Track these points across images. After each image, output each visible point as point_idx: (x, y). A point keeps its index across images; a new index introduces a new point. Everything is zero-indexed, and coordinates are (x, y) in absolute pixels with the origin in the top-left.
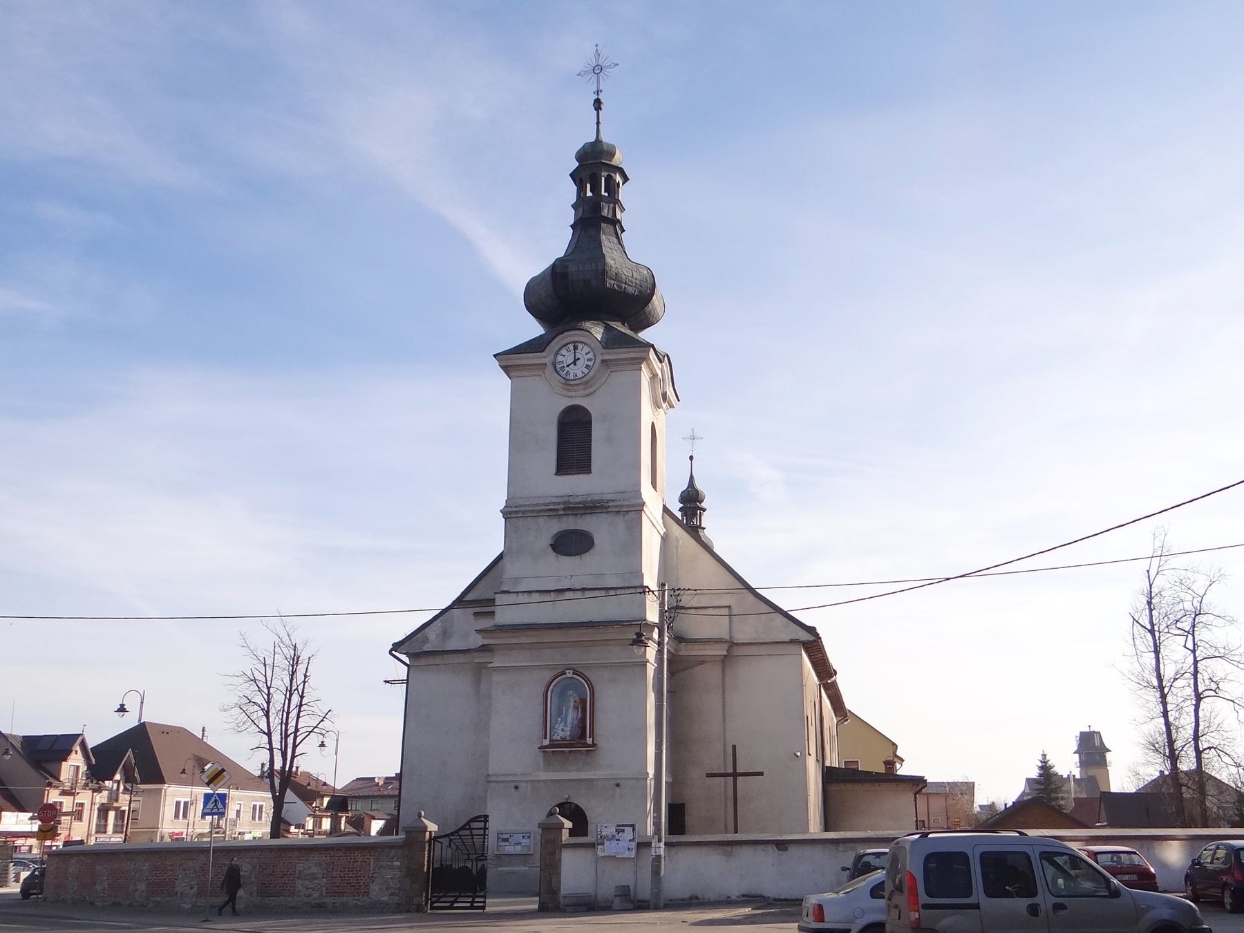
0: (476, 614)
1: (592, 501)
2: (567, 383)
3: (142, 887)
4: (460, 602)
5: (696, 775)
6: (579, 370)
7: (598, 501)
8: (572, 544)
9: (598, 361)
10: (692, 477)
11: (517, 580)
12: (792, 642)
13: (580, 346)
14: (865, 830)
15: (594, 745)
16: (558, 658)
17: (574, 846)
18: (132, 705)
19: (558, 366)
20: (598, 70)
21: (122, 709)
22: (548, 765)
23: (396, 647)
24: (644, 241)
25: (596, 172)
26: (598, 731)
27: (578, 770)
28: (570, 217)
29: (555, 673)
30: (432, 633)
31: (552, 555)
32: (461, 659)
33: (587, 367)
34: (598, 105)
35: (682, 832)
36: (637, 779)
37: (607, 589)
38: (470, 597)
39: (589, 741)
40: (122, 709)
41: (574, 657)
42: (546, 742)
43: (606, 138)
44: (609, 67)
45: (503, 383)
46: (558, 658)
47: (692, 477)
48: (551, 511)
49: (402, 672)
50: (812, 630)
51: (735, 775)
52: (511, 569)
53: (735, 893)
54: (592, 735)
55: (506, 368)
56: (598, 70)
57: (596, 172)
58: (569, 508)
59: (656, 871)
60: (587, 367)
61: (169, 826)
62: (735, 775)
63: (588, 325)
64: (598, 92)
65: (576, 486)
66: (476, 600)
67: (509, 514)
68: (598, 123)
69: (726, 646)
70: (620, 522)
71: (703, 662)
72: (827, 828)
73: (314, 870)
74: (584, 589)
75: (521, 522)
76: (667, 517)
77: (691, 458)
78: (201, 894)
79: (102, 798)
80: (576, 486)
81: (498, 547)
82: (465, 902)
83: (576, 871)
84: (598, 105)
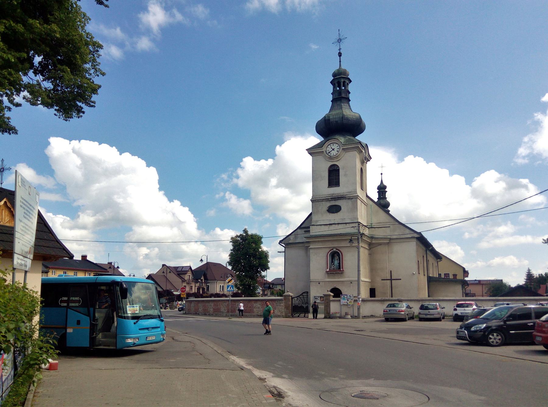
0: (305, 231)
2: (331, 158)
3: (212, 310)
4: (300, 227)
5: (379, 279)
6: (334, 153)
8: (334, 209)
9: (341, 148)
10: (382, 181)
11: (317, 221)
12: (412, 238)
13: (328, 152)
14: (443, 297)
16: (331, 245)
17: (372, 301)
18: (204, 259)
19: (328, 152)
20: (340, 40)
21: (201, 260)
22: (329, 277)
23: (281, 242)
24: (357, 107)
25: (340, 83)
28: (331, 97)
30: (292, 237)
31: (328, 214)
32: (301, 245)
34: (340, 55)
35: (375, 297)
37: (346, 223)
39: (342, 269)
40: (201, 260)
41: (336, 245)
42: (328, 270)
43: (343, 67)
44: (344, 39)
45: (310, 158)
46: (331, 245)
47: (382, 181)
49: (283, 249)
50: (420, 233)
51: (391, 280)
52: (314, 218)
53: (27, 282)
54: (342, 268)
55: (310, 154)
56: (340, 40)
57: (340, 83)
59: (359, 309)
62: (391, 280)
63: (337, 137)
64: (340, 49)
65: (335, 191)
66: (305, 226)
67: (313, 201)
68: (340, 61)
70: (350, 202)
71: (381, 245)
72: (429, 296)
73: (259, 306)
74: (338, 224)
75: (317, 203)
77: (382, 174)
78: (228, 312)
79: (198, 285)
80: (335, 191)
81: (311, 211)
82: (302, 315)
83: (334, 307)
84: (340, 55)
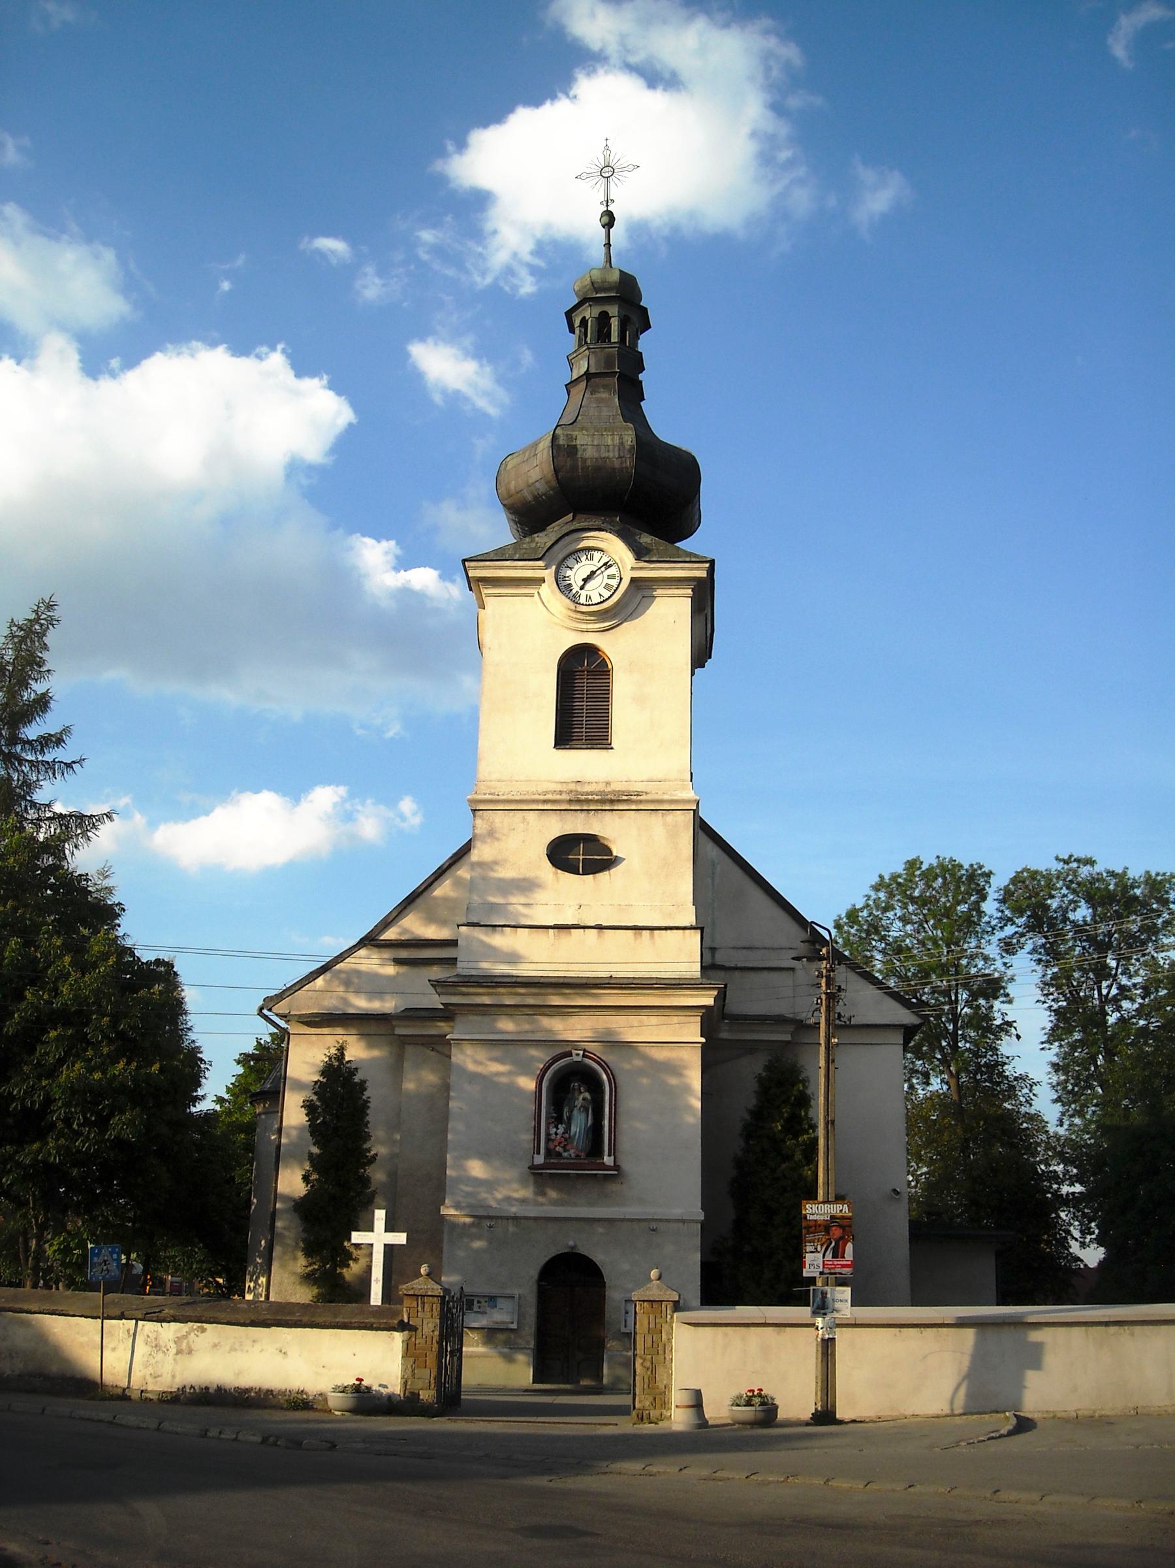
1: (614, 792)
7: (623, 793)
15: (616, 1167)
20: (607, 171)
26: (625, 1143)
27: (591, 1205)
29: (559, 1051)
33: (607, 587)
36: (683, 1221)
38: (390, 934)
39: (608, 1160)
42: (540, 1159)
48: (546, 805)
54: (613, 1151)
56: (607, 171)
58: (579, 801)
60: (607, 587)
61: (809, 1258)
65: (585, 767)
69: (791, 1028)
76: (703, 837)
